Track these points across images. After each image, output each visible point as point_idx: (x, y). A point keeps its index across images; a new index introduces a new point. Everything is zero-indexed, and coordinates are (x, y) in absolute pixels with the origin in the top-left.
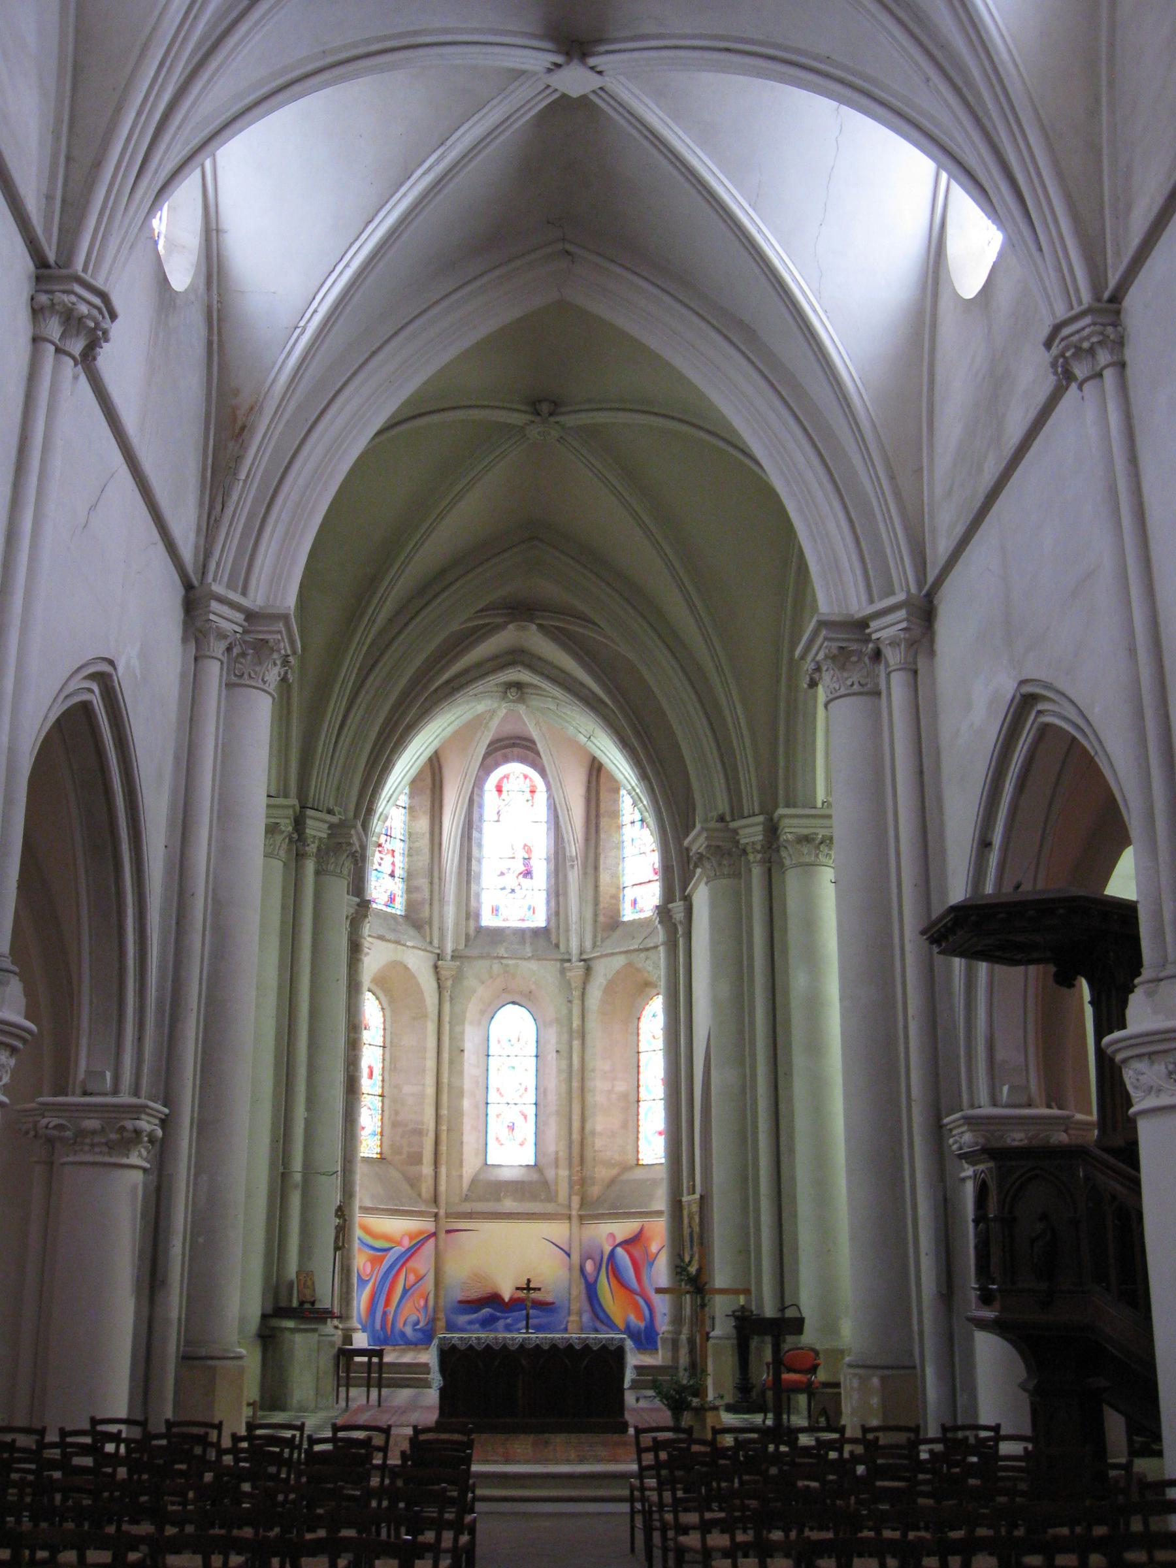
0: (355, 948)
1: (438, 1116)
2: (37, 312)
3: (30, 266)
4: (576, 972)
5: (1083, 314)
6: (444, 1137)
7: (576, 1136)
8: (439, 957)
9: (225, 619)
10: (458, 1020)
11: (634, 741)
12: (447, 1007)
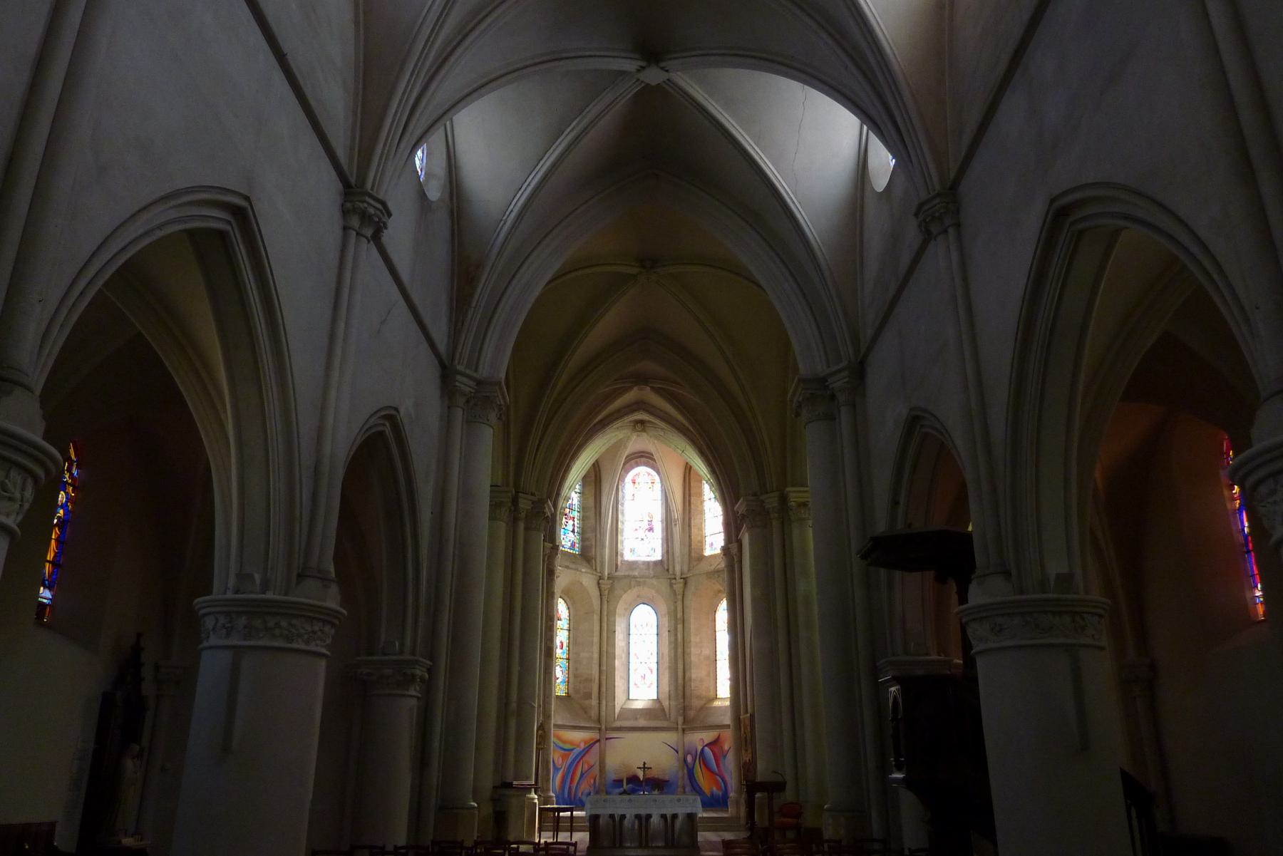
0: (551, 573)
1: (600, 672)
2: (345, 213)
3: (340, 185)
4: (679, 586)
5: (934, 198)
6: (604, 682)
7: (680, 681)
8: (601, 578)
9: (464, 385)
10: (612, 614)
11: (707, 452)
12: (605, 607)
